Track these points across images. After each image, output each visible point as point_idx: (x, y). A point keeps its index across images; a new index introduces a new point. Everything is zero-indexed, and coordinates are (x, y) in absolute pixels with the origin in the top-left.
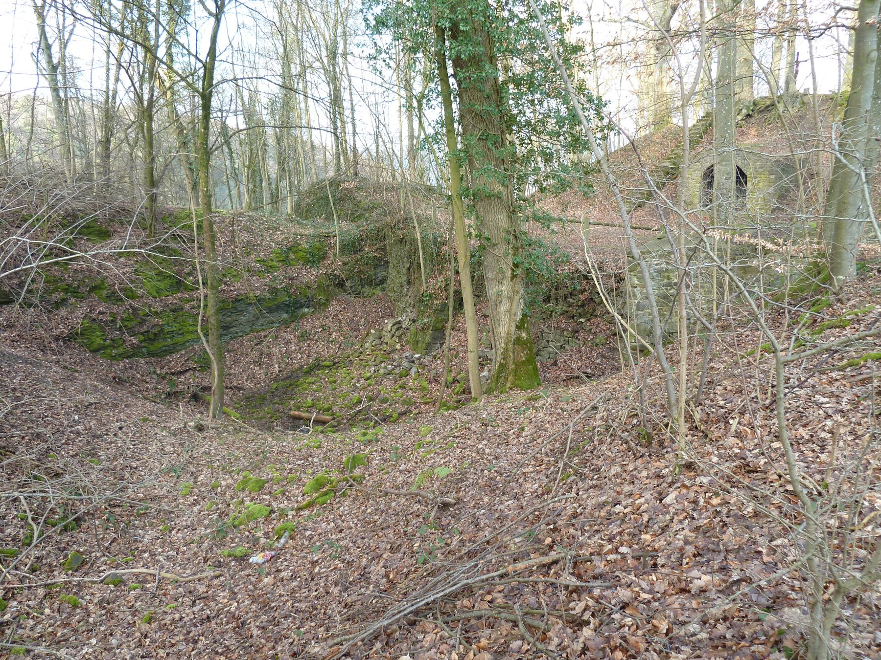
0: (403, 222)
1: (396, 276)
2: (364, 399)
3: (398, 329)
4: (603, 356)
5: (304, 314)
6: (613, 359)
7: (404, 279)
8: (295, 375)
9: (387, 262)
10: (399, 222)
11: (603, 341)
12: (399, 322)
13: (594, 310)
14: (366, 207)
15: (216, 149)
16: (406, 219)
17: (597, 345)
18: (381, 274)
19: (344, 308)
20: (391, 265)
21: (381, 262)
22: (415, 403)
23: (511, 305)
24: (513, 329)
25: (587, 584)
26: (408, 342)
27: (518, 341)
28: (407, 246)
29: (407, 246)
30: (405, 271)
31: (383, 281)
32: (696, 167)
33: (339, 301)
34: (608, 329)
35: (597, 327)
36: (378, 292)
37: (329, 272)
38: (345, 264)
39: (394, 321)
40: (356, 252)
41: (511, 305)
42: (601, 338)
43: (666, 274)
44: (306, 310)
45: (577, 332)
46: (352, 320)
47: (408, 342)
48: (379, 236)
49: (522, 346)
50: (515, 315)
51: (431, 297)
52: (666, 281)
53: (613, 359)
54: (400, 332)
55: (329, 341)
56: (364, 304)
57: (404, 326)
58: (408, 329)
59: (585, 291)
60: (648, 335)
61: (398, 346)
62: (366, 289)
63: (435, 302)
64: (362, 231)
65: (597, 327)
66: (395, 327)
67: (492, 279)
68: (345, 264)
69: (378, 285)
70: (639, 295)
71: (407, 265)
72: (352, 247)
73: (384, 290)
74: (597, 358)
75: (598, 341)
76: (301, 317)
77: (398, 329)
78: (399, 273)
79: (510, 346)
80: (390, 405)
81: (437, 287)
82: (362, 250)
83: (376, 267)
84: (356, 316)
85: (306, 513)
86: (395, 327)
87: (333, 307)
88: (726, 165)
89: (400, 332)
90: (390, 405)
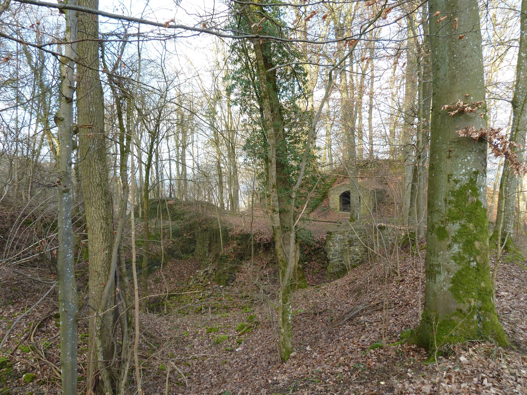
1: (200, 248)
3: (206, 275)
4: (319, 278)
5: (155, 270)
7: (206, 249)
9: (196, 241)
10: (203, 220)
12: (207, 271)
20: (198, 242)
21: (193, 241)
22: (230, 308)
24: (297, 264)
25: (499, 245)
26: (214, 280)
30: (207, 245)
31: (194, 250)
36: (190, 256)
38: (174, 243)
39: (204, 271)
40: (179, 236)
42: (316, 270)
44: (156, 267)
46: (179, 271)
47: (214, 280)
48: (191, 228)
51: (226, 257)
61: (209, 283)
62: (185, 255)
63: (229, 259)
64: (182, 225)
68: (174, 243)
71: (208, 242)
72: (177, 234)
76: (154, 272)
82: (182, 235)
83: (190, 243)
86: (205, 274)
87: (170, 264)
90: (217, 310)
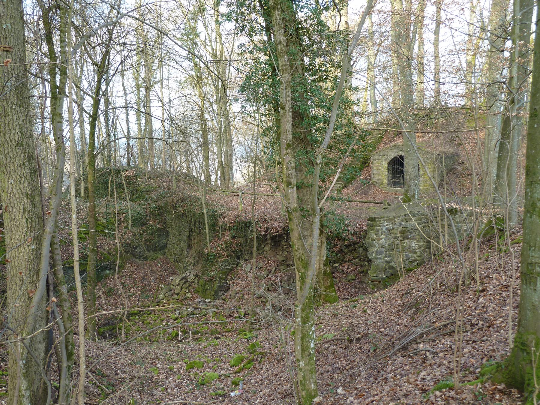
0: (182, 201)
2: (180, 333)
3: (185, 283)
5: (107, 275)
6: (362, 288)
7: (184, 245)
8: (111, 322)
9: (168, 232)
10: (179, 201)
11: (354, 277)
12: (185, 278)
13: (344, 258)
14: (143, 190)
15: (98, 154)
16: (183, 199)
17: (349, 281)
18: (163, 241)
19: (136, 269)
20: (171, 234)
21: (163, 233)
23: (321, 251)
24: (322, 266)
27: (325, 272)
28: (188, 219)
29: (188, 219)
30: (185, 238)
31: (165, 245)
32: (383, 158)
33: (131, 264)
34: (356, 269)
35: (348, 269)
36: (160, 255)
37: (123, 241)
39: (181, 277)
40: (143, 225)
41: (321, 251)
43: (393, 231)
44: (108, 272)
45: (334, 273)
46: (144, 278)
48: (161, 212)
49: (327, 276)
50: (323, 257)
51: (215, 256)
52: (393, 235)
53: (362, 288)
54: (187, 285)
55: (129, 295)
56: (150, 266)
57: (189, 280)
58: (192, 282)
59: (337, 245)
60: (384, 271)
61: (189, 295)
62: (151, 254)
63: (219, 260)
64: (146, 208)
65: (348, 269)
66: (183, 281)
67: (307, 236)
69: (160, 250)
70: (377, 245)
71: (187, 234)
73: (164, 254)
74: (351, 289)
75: (350, 278)
77: (185, 283)
78: (179, 240)
79: (321, 276)
80: (202, 335)
81: (219, 249)
82: (147, 224)
83: (159, 236)
84: (147, 275)
85: (241, 374)
86: (183, 281)
87: (129, 269)
88: (411, 159)
89: (187, 285)
90: (202, 335)
